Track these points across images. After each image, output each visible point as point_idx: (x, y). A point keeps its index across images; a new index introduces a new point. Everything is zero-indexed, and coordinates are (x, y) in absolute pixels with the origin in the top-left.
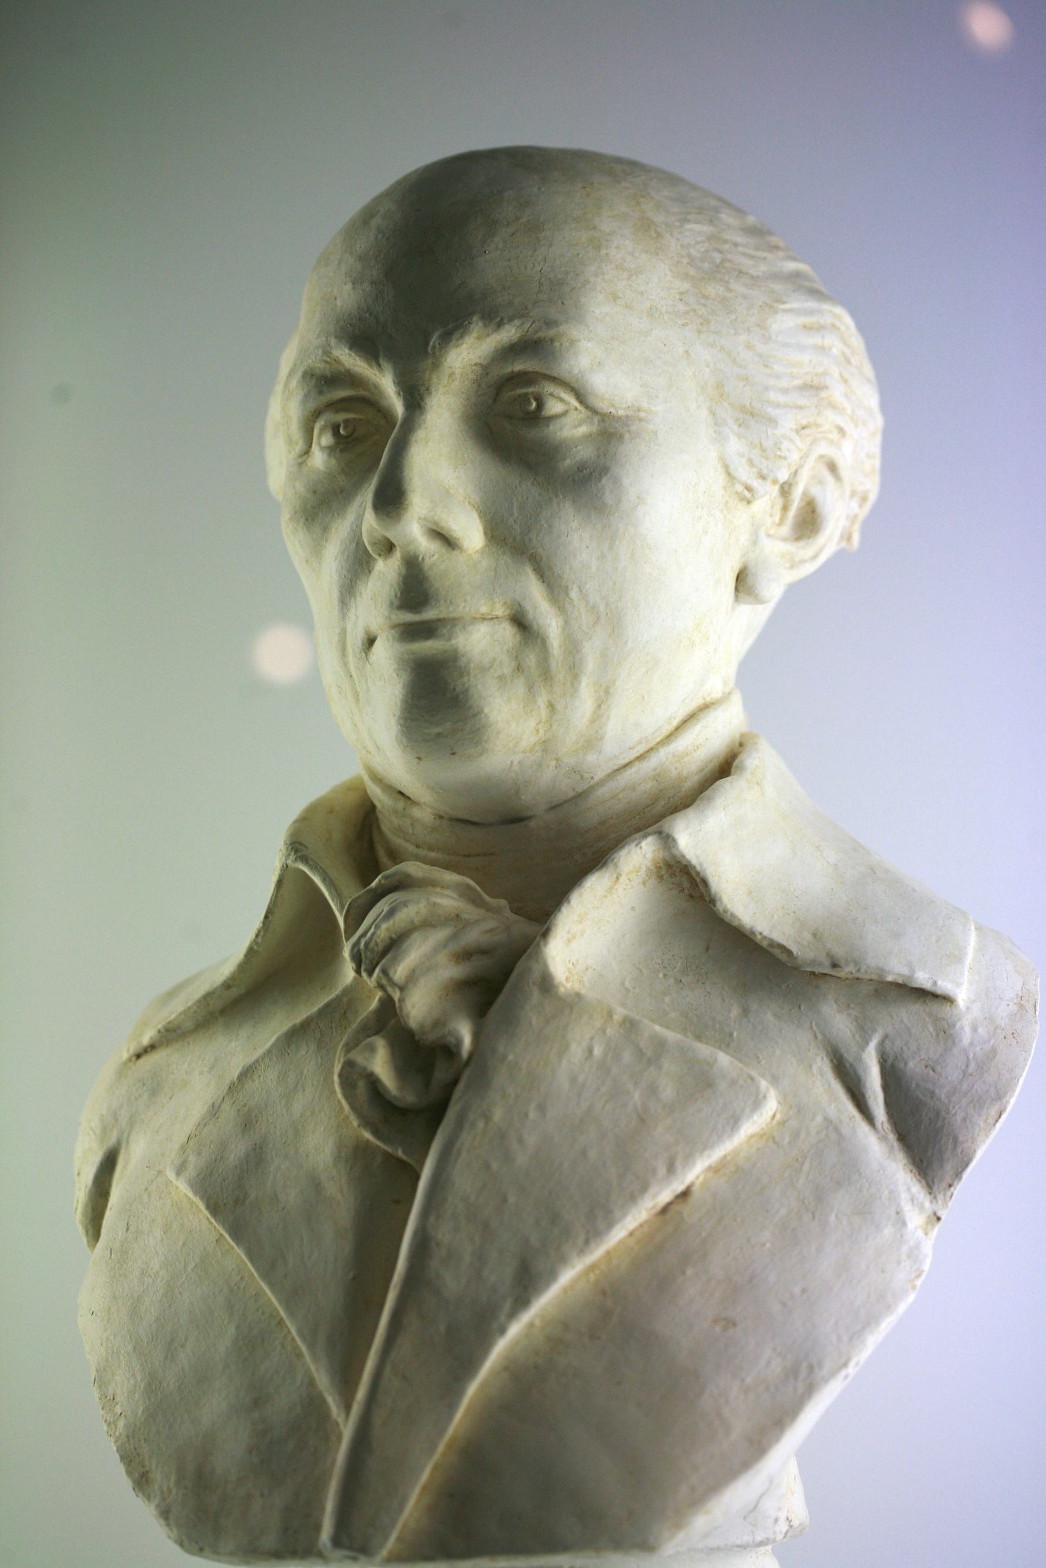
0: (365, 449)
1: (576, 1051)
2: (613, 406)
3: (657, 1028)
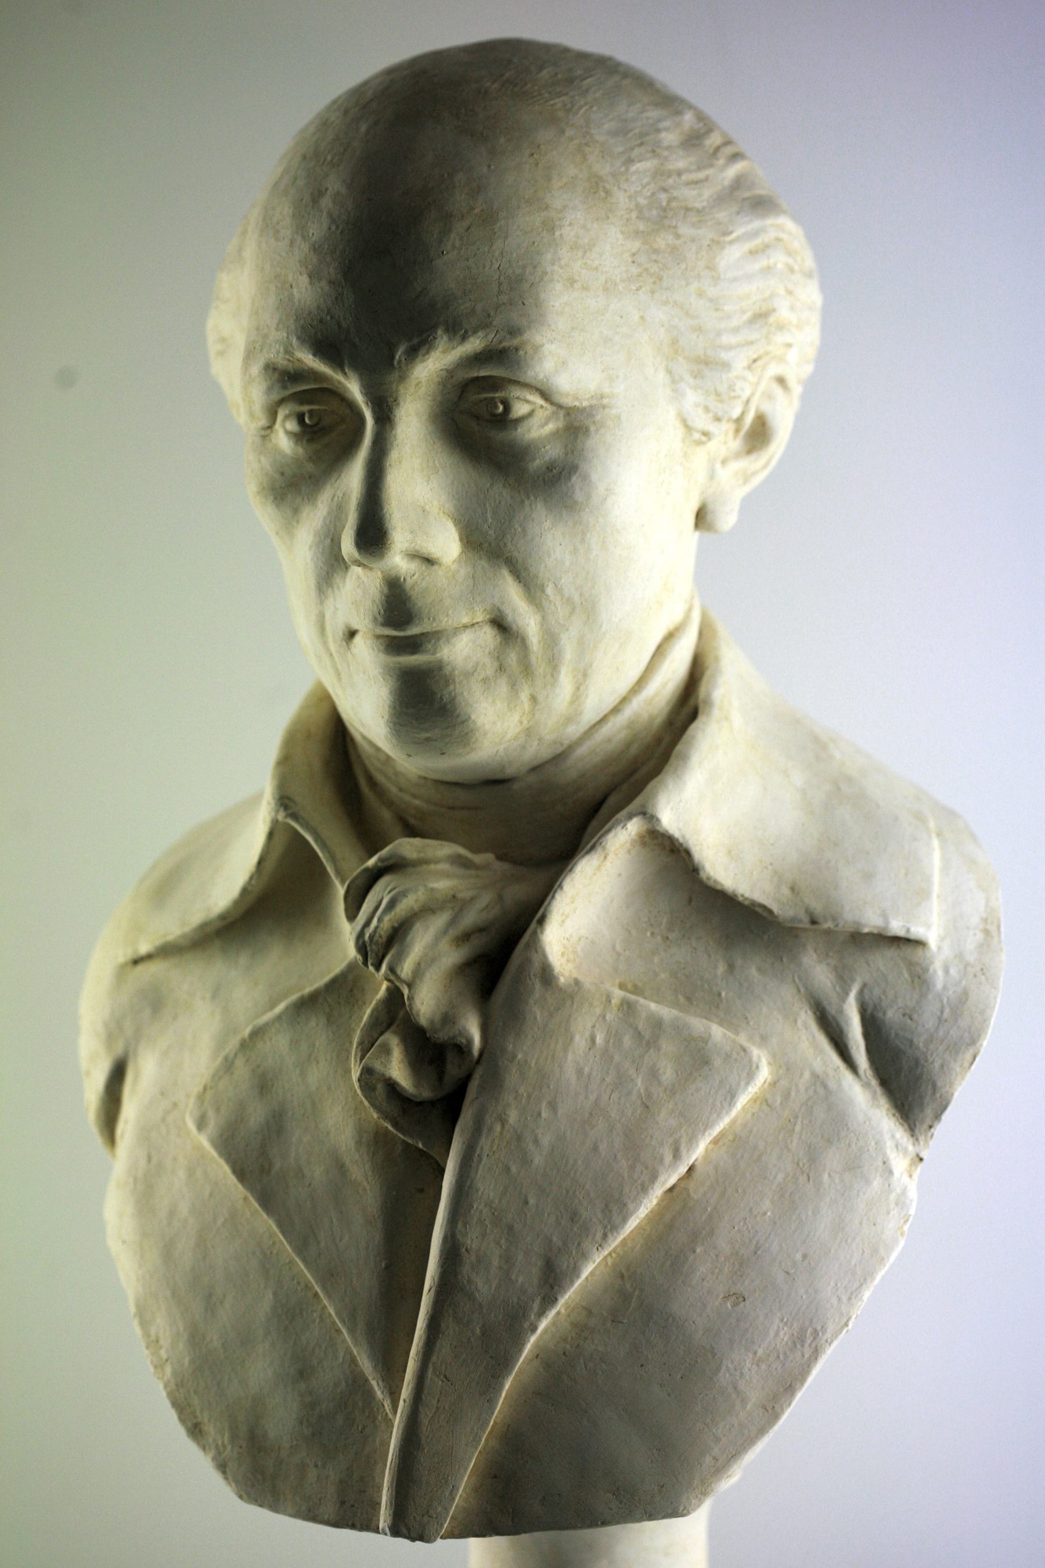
0: (326, 427)
1: (580, 1042)
2: (577, 399)
3: (653, 1006)
